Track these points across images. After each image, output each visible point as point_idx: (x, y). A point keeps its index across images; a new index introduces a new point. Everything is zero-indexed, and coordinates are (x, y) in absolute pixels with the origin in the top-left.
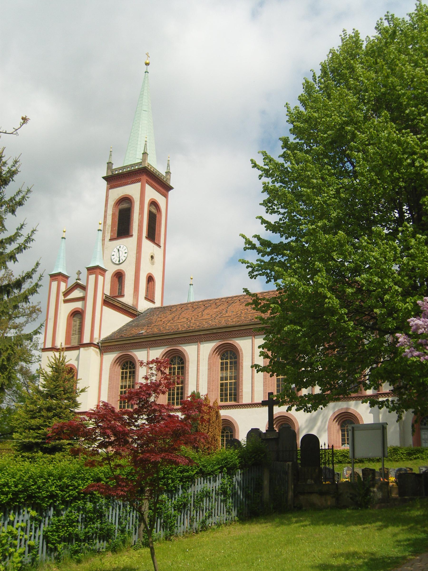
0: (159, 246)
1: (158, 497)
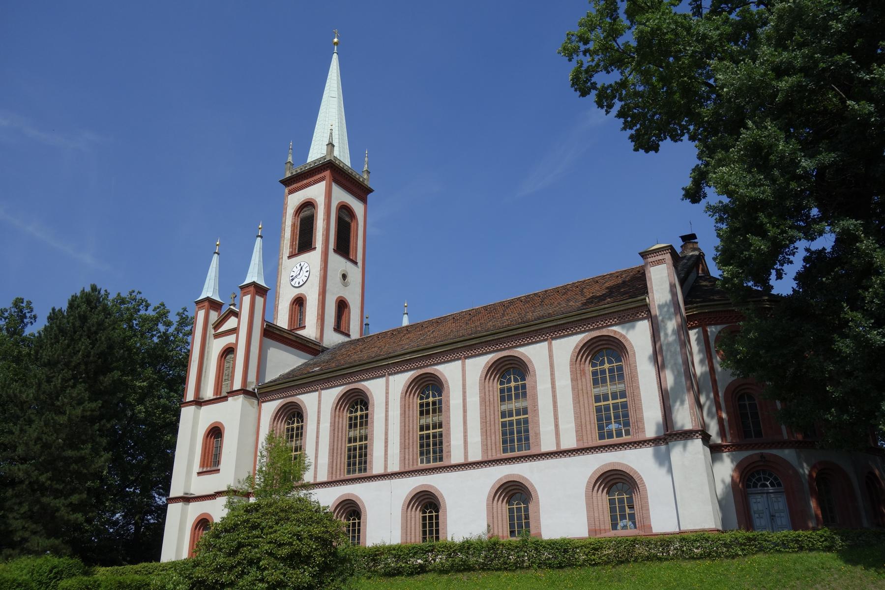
0: (355, 263)
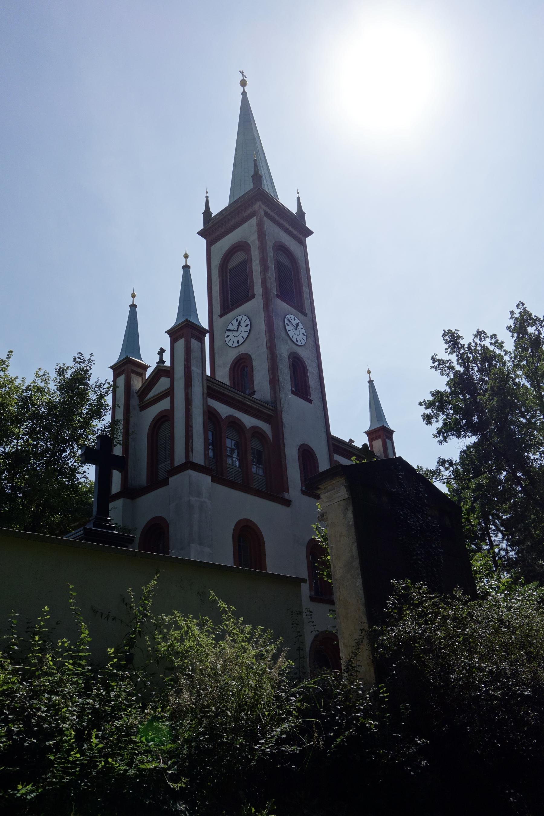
0: (305, 315)
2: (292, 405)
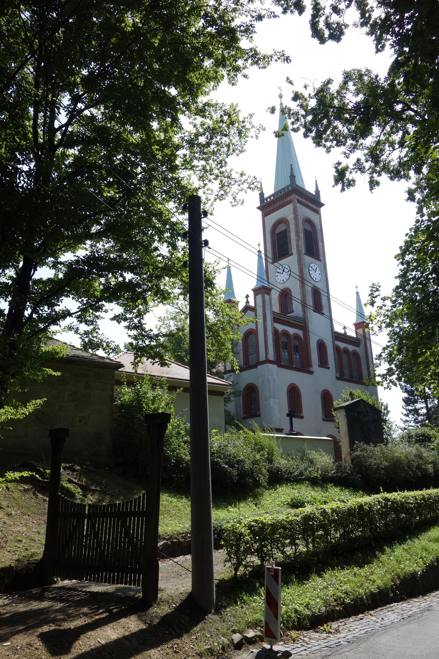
0: (320, 261)
1: (129, 324)
2: (314, 319)
